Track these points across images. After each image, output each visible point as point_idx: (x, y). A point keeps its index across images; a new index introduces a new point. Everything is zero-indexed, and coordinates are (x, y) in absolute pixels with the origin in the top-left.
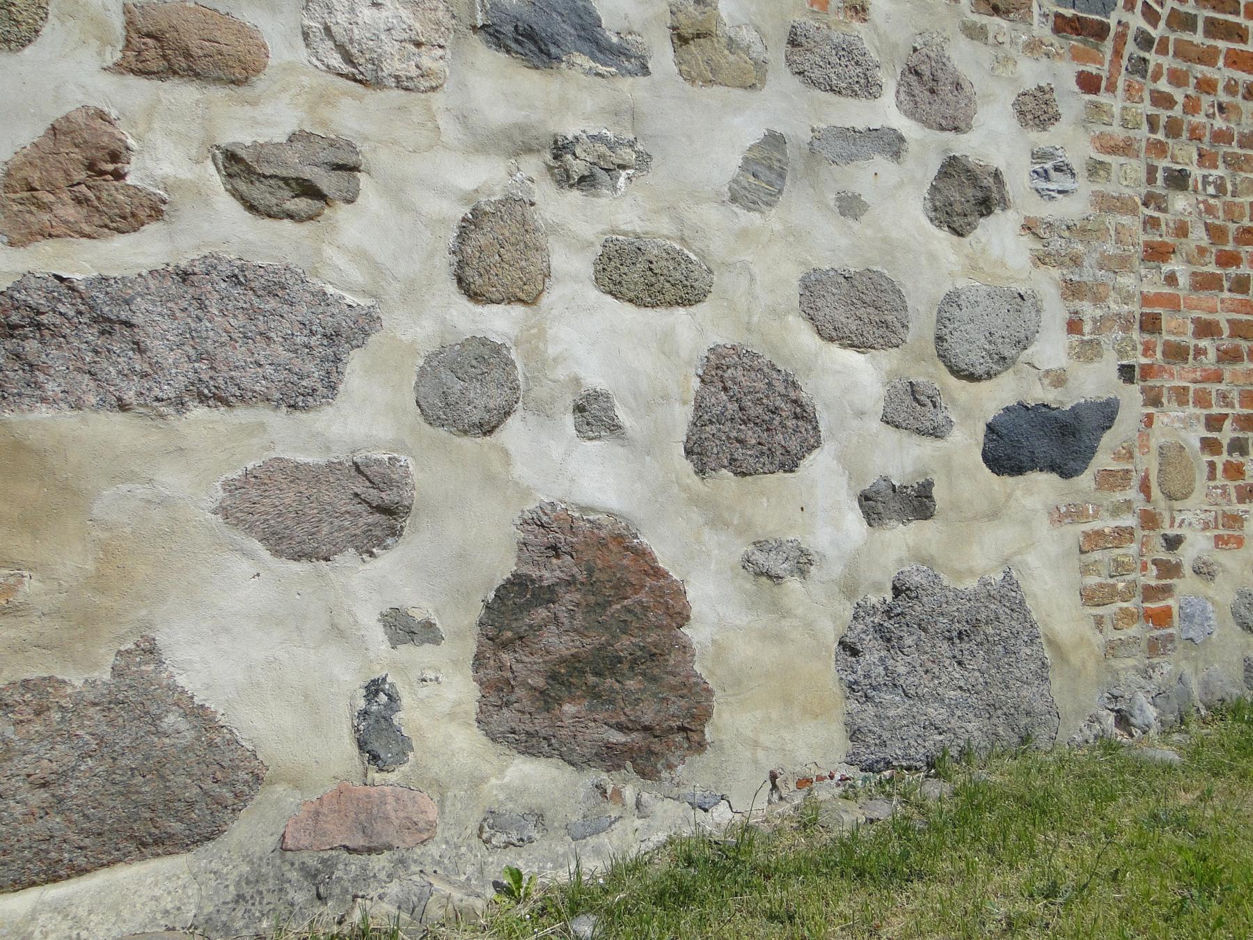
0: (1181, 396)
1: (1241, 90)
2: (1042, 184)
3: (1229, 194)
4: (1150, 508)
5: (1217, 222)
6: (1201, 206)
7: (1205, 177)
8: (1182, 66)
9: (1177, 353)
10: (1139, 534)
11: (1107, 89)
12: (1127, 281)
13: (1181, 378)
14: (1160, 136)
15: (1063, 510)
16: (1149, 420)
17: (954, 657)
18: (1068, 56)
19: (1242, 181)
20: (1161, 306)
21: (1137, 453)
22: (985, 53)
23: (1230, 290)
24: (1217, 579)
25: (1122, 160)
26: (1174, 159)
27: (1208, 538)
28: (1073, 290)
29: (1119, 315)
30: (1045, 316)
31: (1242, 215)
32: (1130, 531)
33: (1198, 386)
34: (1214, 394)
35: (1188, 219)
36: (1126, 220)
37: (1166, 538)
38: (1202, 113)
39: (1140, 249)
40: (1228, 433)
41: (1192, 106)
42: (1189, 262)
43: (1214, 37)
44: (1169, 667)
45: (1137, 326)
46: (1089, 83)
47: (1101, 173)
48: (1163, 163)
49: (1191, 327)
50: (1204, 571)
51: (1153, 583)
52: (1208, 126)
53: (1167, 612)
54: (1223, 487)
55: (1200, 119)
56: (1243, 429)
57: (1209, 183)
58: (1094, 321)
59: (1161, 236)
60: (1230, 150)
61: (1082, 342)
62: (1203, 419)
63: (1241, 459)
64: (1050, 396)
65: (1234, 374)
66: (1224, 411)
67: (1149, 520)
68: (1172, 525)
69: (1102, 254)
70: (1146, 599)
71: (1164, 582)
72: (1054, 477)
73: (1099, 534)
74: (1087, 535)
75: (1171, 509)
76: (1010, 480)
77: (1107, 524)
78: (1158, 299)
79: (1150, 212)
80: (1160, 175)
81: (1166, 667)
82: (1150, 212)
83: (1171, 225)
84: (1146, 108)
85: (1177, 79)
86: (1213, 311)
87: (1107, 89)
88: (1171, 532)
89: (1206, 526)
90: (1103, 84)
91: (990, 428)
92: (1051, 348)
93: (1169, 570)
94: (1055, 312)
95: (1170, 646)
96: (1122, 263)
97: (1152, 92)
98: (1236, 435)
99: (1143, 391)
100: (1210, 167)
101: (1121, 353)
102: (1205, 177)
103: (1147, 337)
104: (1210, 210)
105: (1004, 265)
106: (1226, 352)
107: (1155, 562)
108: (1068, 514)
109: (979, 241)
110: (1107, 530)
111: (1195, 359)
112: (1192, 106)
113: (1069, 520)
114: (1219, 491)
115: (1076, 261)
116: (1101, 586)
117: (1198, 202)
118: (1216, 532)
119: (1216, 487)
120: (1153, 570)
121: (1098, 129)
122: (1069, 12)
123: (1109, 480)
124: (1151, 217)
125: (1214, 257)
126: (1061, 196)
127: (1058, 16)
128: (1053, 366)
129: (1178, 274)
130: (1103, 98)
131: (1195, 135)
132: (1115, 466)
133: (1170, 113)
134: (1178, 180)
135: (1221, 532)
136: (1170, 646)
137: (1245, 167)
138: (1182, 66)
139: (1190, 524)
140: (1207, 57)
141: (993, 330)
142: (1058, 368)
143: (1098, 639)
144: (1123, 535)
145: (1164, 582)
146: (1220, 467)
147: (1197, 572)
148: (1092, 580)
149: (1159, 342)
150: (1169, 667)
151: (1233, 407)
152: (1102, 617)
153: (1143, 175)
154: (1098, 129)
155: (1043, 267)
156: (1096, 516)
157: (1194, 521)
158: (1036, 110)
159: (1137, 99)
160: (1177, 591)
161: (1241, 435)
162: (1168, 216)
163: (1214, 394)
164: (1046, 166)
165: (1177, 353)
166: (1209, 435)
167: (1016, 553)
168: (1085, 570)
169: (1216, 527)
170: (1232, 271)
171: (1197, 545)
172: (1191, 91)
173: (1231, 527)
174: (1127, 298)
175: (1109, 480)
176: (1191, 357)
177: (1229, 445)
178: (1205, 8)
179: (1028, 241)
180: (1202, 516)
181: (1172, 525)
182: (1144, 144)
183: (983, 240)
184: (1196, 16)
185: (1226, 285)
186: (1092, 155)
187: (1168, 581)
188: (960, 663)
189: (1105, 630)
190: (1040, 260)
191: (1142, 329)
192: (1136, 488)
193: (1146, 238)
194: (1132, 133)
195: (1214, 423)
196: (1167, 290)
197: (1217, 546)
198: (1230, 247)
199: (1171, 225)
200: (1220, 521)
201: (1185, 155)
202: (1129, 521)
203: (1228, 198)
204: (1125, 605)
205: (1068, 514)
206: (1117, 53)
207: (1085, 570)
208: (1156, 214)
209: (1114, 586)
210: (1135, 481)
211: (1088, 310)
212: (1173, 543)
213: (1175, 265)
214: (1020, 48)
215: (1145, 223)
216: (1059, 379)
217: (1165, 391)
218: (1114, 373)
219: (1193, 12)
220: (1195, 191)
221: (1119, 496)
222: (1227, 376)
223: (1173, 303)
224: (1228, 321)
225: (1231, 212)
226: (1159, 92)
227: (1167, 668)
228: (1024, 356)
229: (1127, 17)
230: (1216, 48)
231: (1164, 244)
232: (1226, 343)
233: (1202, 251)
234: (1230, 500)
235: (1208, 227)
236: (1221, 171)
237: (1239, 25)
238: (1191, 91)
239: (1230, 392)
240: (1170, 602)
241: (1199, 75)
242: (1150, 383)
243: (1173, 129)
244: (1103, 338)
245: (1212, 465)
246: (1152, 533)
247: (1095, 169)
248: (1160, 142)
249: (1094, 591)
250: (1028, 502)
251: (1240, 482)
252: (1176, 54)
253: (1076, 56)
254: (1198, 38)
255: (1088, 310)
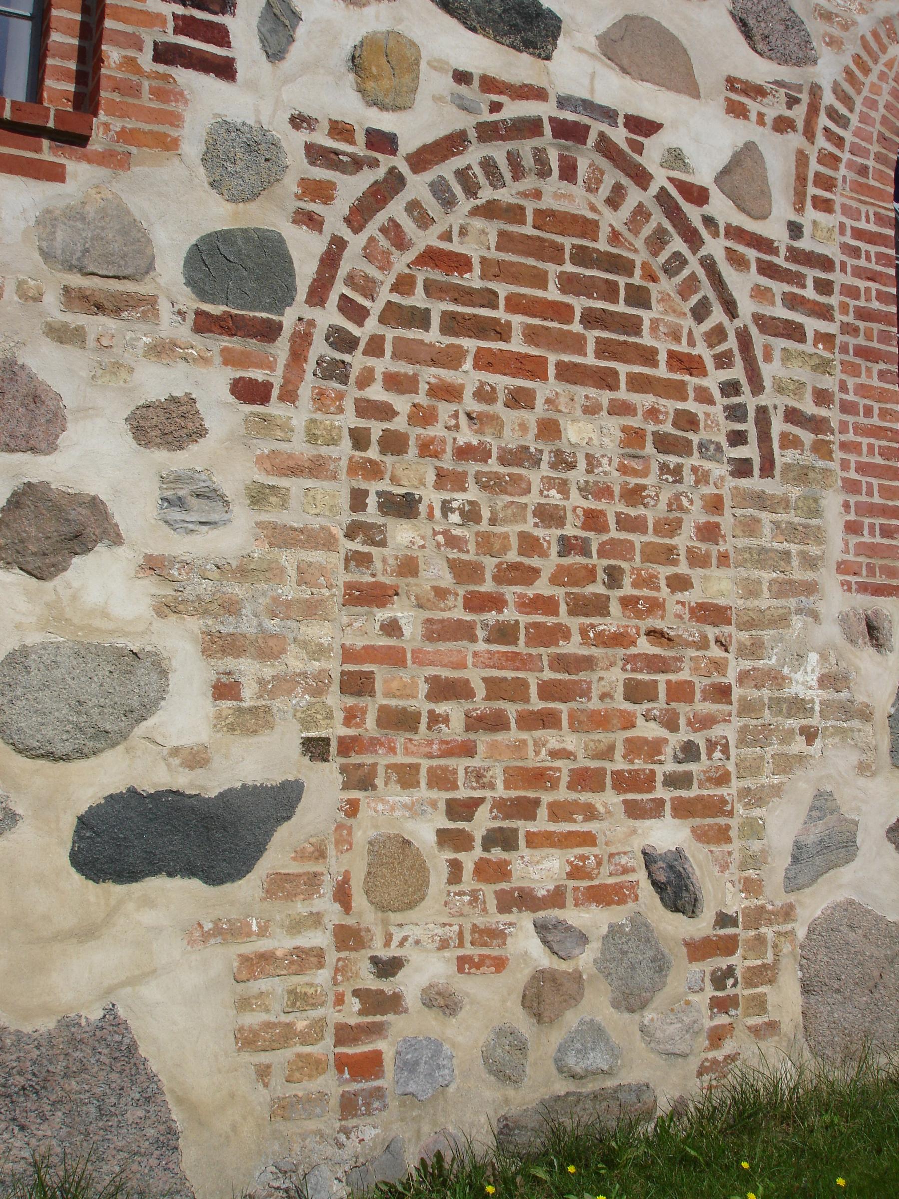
0: (406, 777)
1: (502, 397)
2: (176, 514)
3: (485, 521)
4: (350, 921)
5: (464, 556)
6: (440, 538)
7: (444, 502)
8: (404, 368)
9: (400, 721)
10: (332, 956)
11: (281, 398)
12: (319, 632)
13: (407, 752)
14: (373, 453)
15: (208, 926)
16: (352, 808)
17: (14, 1119)
18: (218, 359)
19: (506, 507)
20: (373, 662)
21: (331, 851)
22: (79, 360)
23: (488, 641)
24: (462, 1014)
25: (309, 483)
26: (394, 480)
27: (448, 960)
28: (218, 645)
29: (304, 675)
30: (174, 679)
31: (505, 548)
32: (319, 954)
33: (435, 763)
34: (461, 773)
35: (420, 554)
36: (316, 556)
37: (375, 960)
38: (440, 425)
39: (339, 591)
40: (483, 822)
41: (422, 416)
42: (420, 606)
43: (457, 335)
44: (374, 1132)
45: (335, 687)
46: (250, 392)
47: (273, 499)
48: (374, 487)
49: (423, 688)
50: (442, 1002)
51: (353, 1021)
52: (450, 441)
53: (375, 1059)
54: (474, 894)
55: (435, 431)
56: (508, 816)
57: (453, 510)
58: (261, 682)
59: (373, 575)
60: (486, 469)
61: (240, 710)
62: (442, 806)
63: (505, 856)
64: (183, 781)
65: (494, 746)
66: (477, 794)
67: (348, 938)
68: (387, 944)
69: (275, 599)
70: (338, 1042)
71: (370, 1019)
72: (195, 884)
73: (266, 958)
74: (245, 959)
75: (385, 923)
76: (118, 890)
77: (281, 943)
78: (370, 654)
79: (356, 545)
80: (372, 501)
81: (369, 1132)
82: (356, 545)
83: (391, 561)
84: (349, 419)
85: (393, 382)
86: (463, 666)
87: (281, 398)
88: (384, 954)
89: (444, 945)
90: (275, 392)
91: (81, 819)
92: (185, 715)
93: (381, 1003)
94: (190, 675)
95: (376, 1104)
96: (312, 609)
97: (357, 401)
98: (497, 824)
99: (343, 770)
100: (453, 490)
101: (306, 724)
102: (444, 502)
103: (350, 701)
104: (452, 541)
105: (105, 615)
106: (480, 719)
107: (356, 993)
108: (217, 931)
109: (69, 585)
110: (279, 953)
111: (429, 728)
112: (422, 416)
113: (219, 939)
114: (467, 898)
115: (231, 608)
116: (268, 1025)
117: (435, 533)
118: (461, 952)
119: (461, 894)
120: (356, 1004)
121: (265, 447)
122: (216, 310)
123: (281, 886)
124: (356, 552)
125: (461, 600)
126: (205, 528)
127: (199, 313)
128: (187, 741)
129: (402, 623)
130: (275, 408)
131: (427, 449)
132: (294, 868)
133: (386, 425)
134: (403, 506)
135: (469, 950)
136: (376, 1104)
137: (510, 488)
138: (404, 368)
139: (417, 942)
140: (451, 358)
141: (83, 698)
142: (188, 741)
143: (260, 1096)
144: (307, 959)
145: (370, 1019)
146: (469, 867)
147: (428, 1003)
148: (253, 1019)
149: (371, 707)
150: (374, 1132)
151: (492, 787)
152: (268, 1066)
153: (344, 500)
154: (265, 447)
155: (173, 618)
156: (263, 932)
157: (424, 939)
158: (166, 424)
159: (332, 409)
160: (391, 1032)
161: (506, 824)
162: (385, 551)
163: (461, 773)
164: (181, 493)
165: (400, 721)
166: (451, 825)
167: (131, 982)
168: (244, 1004)
169: (461, 945)
170: (492, 617)
171: (427, 969)
172: (421, 398)
173: (485, 945)
174: (319, 652)
175: (281, 886)
176: (423, 726)
177: (484, 838)
178: (441, 299)
179: (150, 586)
180: (439, 931)
181: (387, 944)
182: (344, 463)
183: (76, 584)
184: (427, 310)
185: (481, 634)
186: (256, 477)
187: (378, 1018)
188: (23, 1128)
189: (273, 1083)
190: (168, 608)
191: (343, 691)
192: (329, 895)
193: (349, 577)
194: (324, 451)
195: (461, 810)
196: (384, 642)
197: (461, 970)
198: (488, 586)
199: (391, 561)
200: (468, 937)
201: (414, 475)
202: (320, 939)
203: (484, 526)
204: (307, 1049)
205: (217, 931)
206: (297, 356)
207: (244, 1004)
208: (366, 549)
209: (289, 1025)
210: (327, 889)
211: (248, 670)
212: (387, 968)
213: (402, 612)
214: (140, 352)
215: (347, 560)
216: (196, 759)
217: (380, 771)
218: (296, 748)
219: (422, 305)
220: (430, 516)
221: (301, 908)
222: (481, 748)
223: (395, 658)
224: (485, 680)
225: (486, 543)
226: (368, 401)
227: (369, 1133)
228: (141, 729)
229: (310, 313)
230: (460, 347)
231: (377, 585)
232: (480, 704)
233: (441, 593)
234: (485, 910)
235: (453, 564)
236: (473, 493)
237: (496, 321)
238: (421, 398)
239: (488, 769)
240: (381, 1045)
241: (432, 380)
242: (355, 759)
243: (393, 443)
244: (277, 704)
245: (456, 867)
246: (353, 955)
247: (258, 496)
248: (370, 461)
249: (256, 1034)
250: (148, 917)
251: (505, 886)
252: (395, 356)
253: (229, 359)
254: (433, 335)
255: (248, 670)
